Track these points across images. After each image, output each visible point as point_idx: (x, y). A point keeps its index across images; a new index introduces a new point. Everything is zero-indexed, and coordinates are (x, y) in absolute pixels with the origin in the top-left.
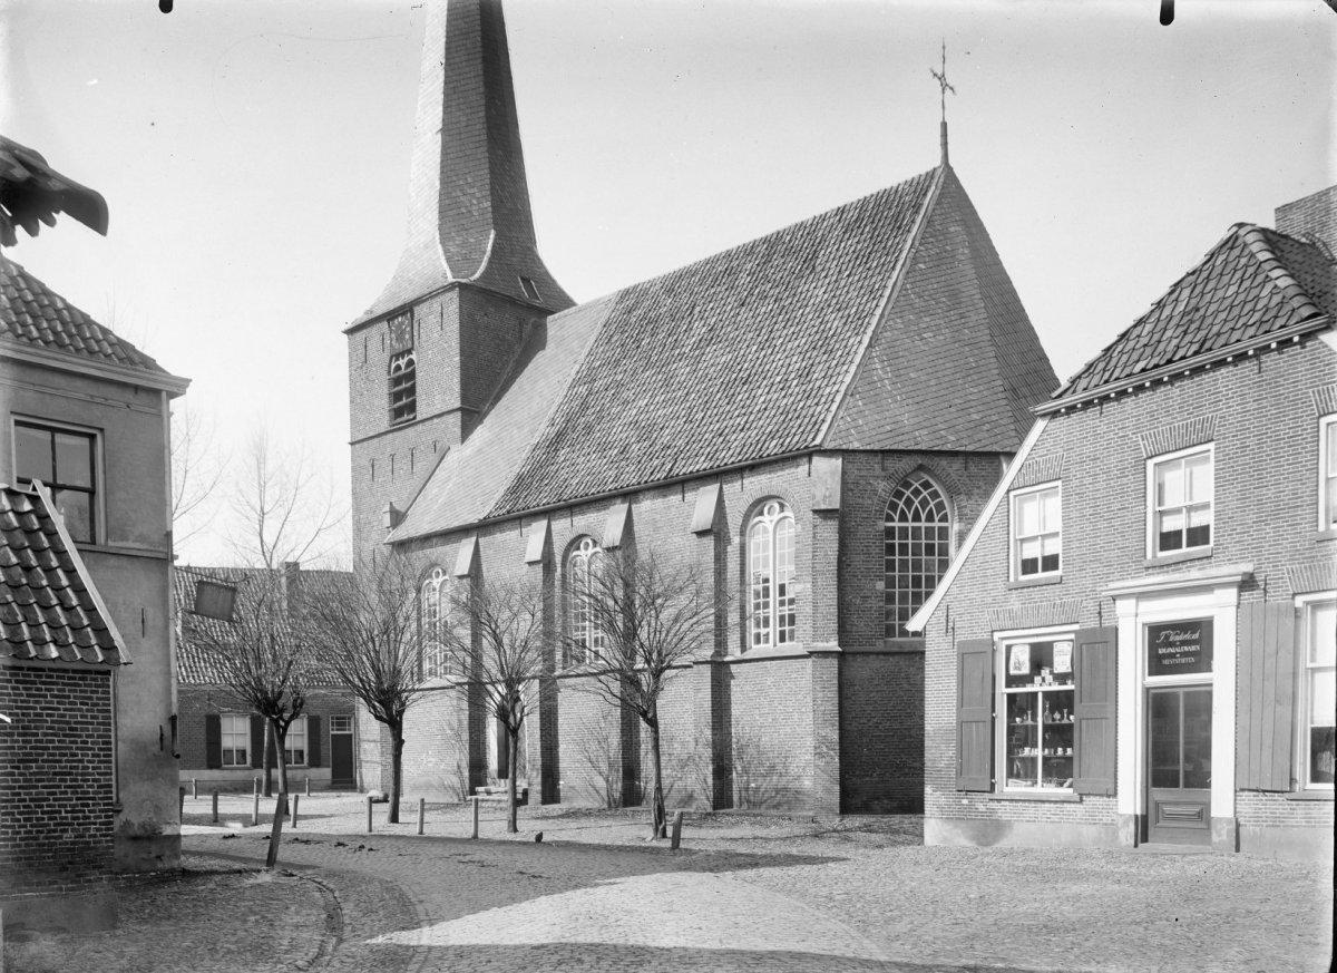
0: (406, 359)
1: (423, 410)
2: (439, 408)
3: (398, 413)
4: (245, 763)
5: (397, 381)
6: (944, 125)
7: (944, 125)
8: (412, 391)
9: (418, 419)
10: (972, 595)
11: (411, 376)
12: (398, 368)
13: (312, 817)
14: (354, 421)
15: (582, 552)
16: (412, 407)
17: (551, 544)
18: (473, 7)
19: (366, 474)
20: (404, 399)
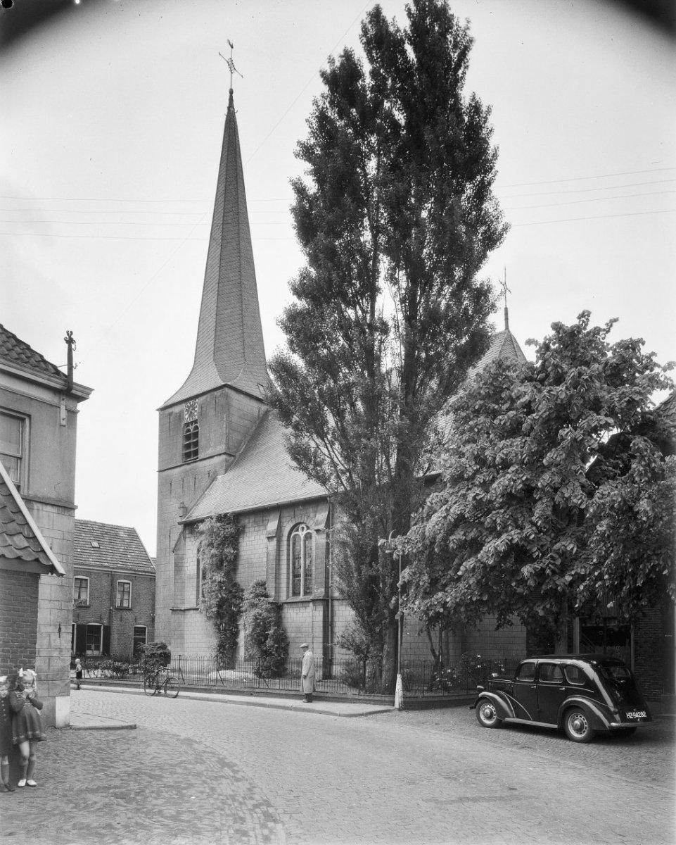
0: (194, 426)
1: (201, 456)
2: (210, 452)
3: (188, 455)
4: (87, 580)
5: (188, 437)
6: (231, 92)
7: (231, 92)
8: (196, 444)
9: (200, 458)
10: (515, 537)
11: (196, 435)
12: (189, 430)
13: (231, 100)
14: (159, 466)
15: (300, 533)
16: (196, 453)
17: (232, 100)
18: (253, 529)
19: (166, 487)
20: (191, 451)
